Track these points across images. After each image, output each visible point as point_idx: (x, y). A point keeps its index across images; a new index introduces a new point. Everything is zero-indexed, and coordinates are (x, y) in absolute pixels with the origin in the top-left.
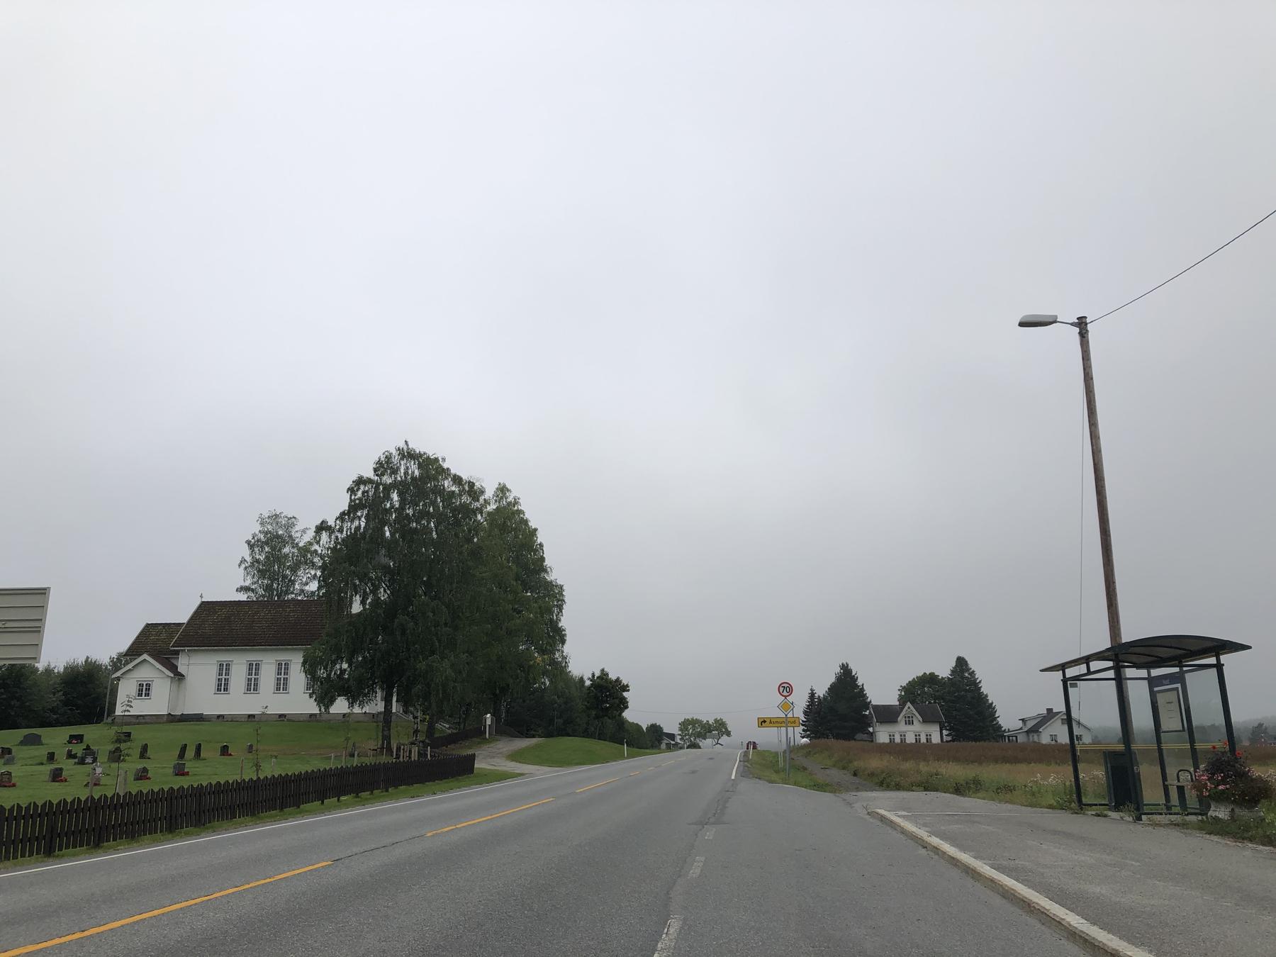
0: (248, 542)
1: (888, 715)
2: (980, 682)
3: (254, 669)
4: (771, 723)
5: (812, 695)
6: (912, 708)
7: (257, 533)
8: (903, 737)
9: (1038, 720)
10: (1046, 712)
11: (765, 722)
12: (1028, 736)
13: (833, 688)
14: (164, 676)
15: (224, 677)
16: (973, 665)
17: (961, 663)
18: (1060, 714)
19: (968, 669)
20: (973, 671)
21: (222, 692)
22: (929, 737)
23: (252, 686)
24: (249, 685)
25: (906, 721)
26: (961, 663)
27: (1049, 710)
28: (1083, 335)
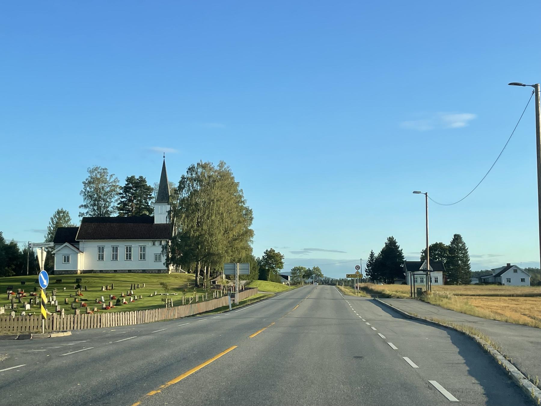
0: (84, 183)
1: (414, 266)
2: (467, 249)
4: (351, 276)
5: (372, 255)
7: (88, 178)
8: (422, 279)
9: (503, 269)
10: (506, 266)
11: (349, 276)
13: (383, 252)
14: (75, 253)
16: (464, 240)
17: (457, 239)
18: (513, 267)
19: (461, 242)
20: (465, 243)
23: (129, 257)
24: (127, 256)
26: (457, 239)
28: (426, 196)
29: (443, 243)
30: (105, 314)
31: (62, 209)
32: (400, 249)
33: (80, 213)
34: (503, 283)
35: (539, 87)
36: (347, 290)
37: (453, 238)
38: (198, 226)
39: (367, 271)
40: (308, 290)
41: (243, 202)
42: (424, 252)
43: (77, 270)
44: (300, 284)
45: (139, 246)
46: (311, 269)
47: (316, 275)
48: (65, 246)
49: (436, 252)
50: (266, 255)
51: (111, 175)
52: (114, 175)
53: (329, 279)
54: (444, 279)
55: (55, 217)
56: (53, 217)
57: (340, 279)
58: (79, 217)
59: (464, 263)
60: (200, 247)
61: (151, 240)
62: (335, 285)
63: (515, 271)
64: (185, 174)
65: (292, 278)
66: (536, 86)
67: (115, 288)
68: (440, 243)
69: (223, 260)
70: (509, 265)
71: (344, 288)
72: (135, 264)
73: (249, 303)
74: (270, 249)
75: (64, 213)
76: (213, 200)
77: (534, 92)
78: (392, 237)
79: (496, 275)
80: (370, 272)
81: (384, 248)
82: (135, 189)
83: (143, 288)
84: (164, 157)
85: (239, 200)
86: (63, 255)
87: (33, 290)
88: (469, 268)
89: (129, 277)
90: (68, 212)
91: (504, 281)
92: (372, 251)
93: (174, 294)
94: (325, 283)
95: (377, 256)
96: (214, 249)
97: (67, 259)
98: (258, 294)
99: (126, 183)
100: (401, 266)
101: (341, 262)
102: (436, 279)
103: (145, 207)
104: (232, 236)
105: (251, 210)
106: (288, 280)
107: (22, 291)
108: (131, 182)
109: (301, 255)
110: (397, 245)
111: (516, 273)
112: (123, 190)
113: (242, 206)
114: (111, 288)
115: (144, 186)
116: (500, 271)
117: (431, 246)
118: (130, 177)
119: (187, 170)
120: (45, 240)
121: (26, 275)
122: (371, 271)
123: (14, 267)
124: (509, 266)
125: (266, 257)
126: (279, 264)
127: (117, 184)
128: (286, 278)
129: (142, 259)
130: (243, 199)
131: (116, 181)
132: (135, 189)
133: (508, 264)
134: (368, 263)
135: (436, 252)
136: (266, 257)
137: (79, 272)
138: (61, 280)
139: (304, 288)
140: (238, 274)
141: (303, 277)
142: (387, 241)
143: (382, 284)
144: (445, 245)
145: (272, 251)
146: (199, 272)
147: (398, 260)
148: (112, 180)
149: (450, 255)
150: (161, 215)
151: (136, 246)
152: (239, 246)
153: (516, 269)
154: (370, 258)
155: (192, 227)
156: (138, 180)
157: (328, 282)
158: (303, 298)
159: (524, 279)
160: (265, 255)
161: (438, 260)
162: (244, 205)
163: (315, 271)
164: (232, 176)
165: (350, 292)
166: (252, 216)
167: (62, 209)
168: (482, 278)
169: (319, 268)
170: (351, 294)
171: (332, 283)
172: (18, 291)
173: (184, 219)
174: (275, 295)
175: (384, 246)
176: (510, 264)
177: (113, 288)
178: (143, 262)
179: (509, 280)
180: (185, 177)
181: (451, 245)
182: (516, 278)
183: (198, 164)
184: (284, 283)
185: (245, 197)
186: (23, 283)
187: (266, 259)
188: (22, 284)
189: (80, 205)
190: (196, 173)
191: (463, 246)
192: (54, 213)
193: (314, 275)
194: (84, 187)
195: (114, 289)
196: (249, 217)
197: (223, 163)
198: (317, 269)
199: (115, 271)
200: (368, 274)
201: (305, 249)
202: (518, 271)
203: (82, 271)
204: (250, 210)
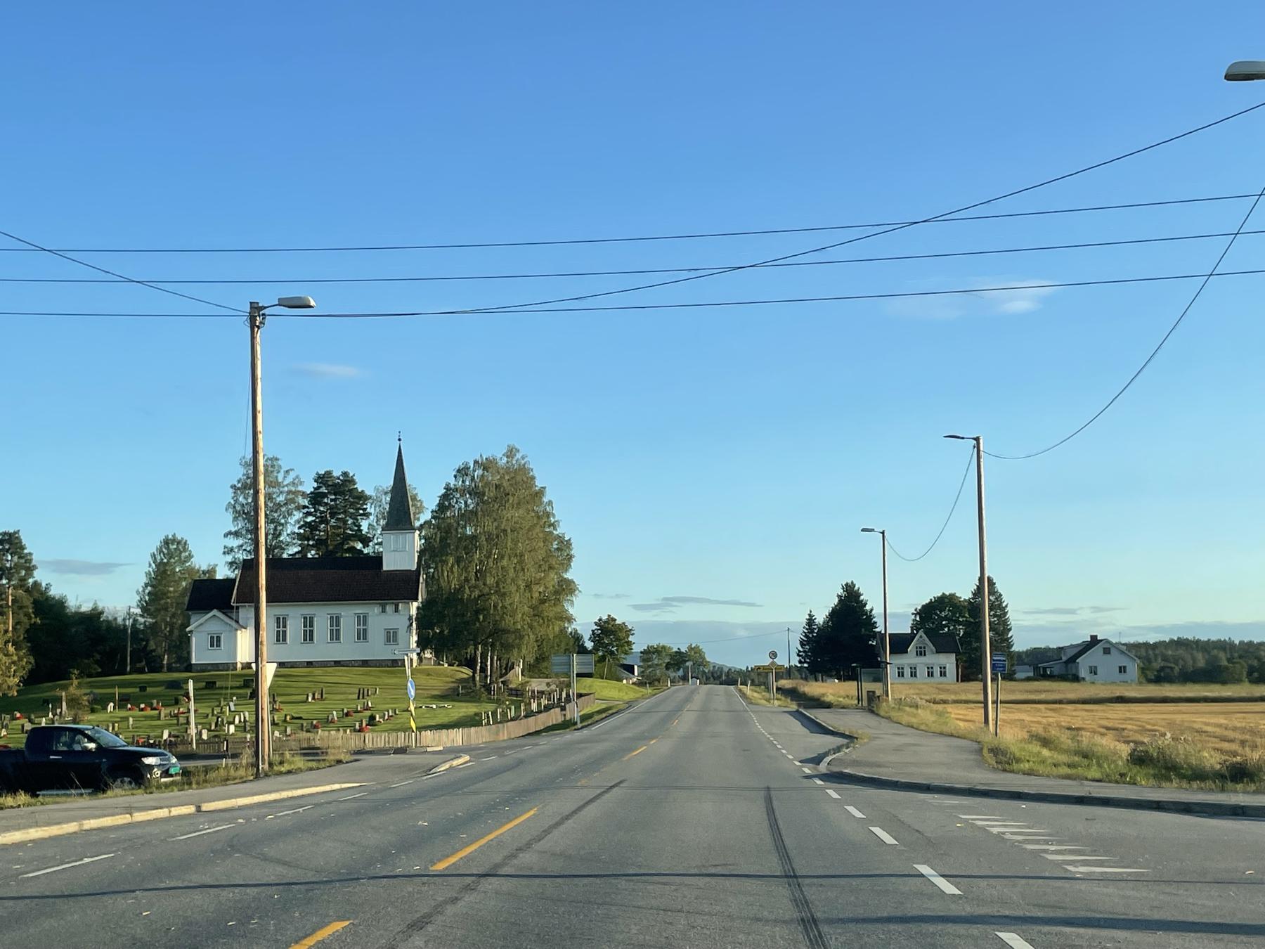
0: (233, 487)
1: (900, 644)
2: (1006, 606)
3: (308, 622)
5: (811, 621)
6: (925, 636)
10: (1089, 640)
12: (1066, 667)
13: (834, 614)
15: (281, 629)
18: (1102, 643)
20: (1001, 595)
21: (392, 643)
22: (943, 670)
23: (335, 636)
25: (917, 652)
27: (1094, 638)
29: (957, 595)
30: (431, 731)
31: (174, 535)
32: (868, 607)
33: (225, 547)
34: (1083, 676)
35: (981, 441)
36: (755, 694)
37: (978, 584)
38: (477, 579)
39: (801, 654)
40: (682, 695)
41: (552, 525)
42: (918, 613)
43: (236, 663)
44: (659, 682)
45: (355, 614)
46: (683, 650)
47: (694, 664)
48: (212, 617)
49: (943, 614)
50: (599, 628)
51: (287, 471)
52: (292, 470)
53: (721, 669)
54: (960, 670)
55: (161, 551)
56: (156, 553)
57: (747, 668)
58: (223, 556)
59: (999, 635)
60: (481, 617)
61: (377, 603)
62: (734, 683)
63: (1107, 651)
64: (452, 482)
65: (642, 670)
66: (977, 439)
67: (327, 695)
68: (950, 595)
69: (525, 642)
70: (1094, 638)
71: (752, 690)
72: (348, 649)
73: (596, 718)
74: (607, 617)
75: (179, 543)
76: (505, 531)
77: (974, 447)
78: (852, 582)
79: (1068, 660)
80: (807, 656)
81: (836, 606)
82: (333, 497)
83: (376, 696)
84: (400, 440)
85: (544, 519)
86: (208, 634)
87: (174, 701)
88: (1009, 646)
89: (340, 674)
90: (186, 541)
91: (1083, 673)
92: (811, 612)
93: (446, 705)
94: (712, 678)
95: (822, 623)
96: (508, 622)
97: (215, 642)
98: (596, 705)
99: (315, 485)
100: (870, 642)
101: (746, 627)
102: (930, 670)
103: (354, 533)
104: (537, 595)
105: (570, 540)
106: (633, 674)
107: (158, 703)
108: (324, 484)
109: (655, 612)
110: (862, 601)
111: (1109, 655)
112: (309, 499)
113: (551, 533)
114: (320, 697)
115: (351, 491)
116: (1075, 651)
117: (933, 600)
118: (323, 473)
119: (454, 473)
120: (139, 598)
121: (124, 673)
122: (810, 654)
123: (98, 657)
124: (1094, 641)
125: (600, 631)
126: (624, 646)
127: (300, 488)
128: (630, 669)
129: (362, 640)
130: (552, 520)
131: (296, 482)
132: (333, 497)
133: (1092, 637)
134: (803, 638)
135: (943, 614)
136: (600, 631)
137: (239, 666)
138: (215, 683)
139: (674, 692)
140: (575, 673)
141: (667, 668)
142: (840, 591)
143: (836, 681)
144: (962, 599)
145: (611, 620)
146: (479, 664)
147: (863, 630)
148: (289, 480)
149: (972, 620)
150: (396, 553)
151: (348, 614)
152: (551, 615)
153: (1107, 646)
154: (807, 627)
155: (467, 580)
156: (339, 479)
157: (720, 677)
158: (679, 709)
159: (1125, 667)
160: (596, 627)
161: (946, 629)
162: (554, 532)
163: (693, 653)
164: (531, 474)
165: (761, 699)
166: (572, 552)
167: (174, 535)
168: (1040, 665)
169: (700, 648)
170: (764, 702)
171: (727, 678)
172: (152, 704)
173: (453, 566)
174: (627, 705)
175: (836, 601)
176: (1096, 636)
177: (324, 697)
178: (362, 645)
179: (1093, 671)
180: (452, 486)
181: (973, 599)
182: (1108, 665)
183: (476, 462)
184: (625, 681)
185: (559, 513)
186: (143, 689)
187: (598, 635)
188: (141, 690)
189: (226, 531)
190: (473, 479)
191: (998, 601)
192: (159, 543)
193: (689, 664)
194: (233, 495)
195: (326, 698)
196: (566, 554)
197: (514, 450)
198: (695, 650)
199: (310, 664)
200: (803, 660)
201: (665, 599)
202: (1112, 650)
203: (244, 665)
204: (567, 541)
